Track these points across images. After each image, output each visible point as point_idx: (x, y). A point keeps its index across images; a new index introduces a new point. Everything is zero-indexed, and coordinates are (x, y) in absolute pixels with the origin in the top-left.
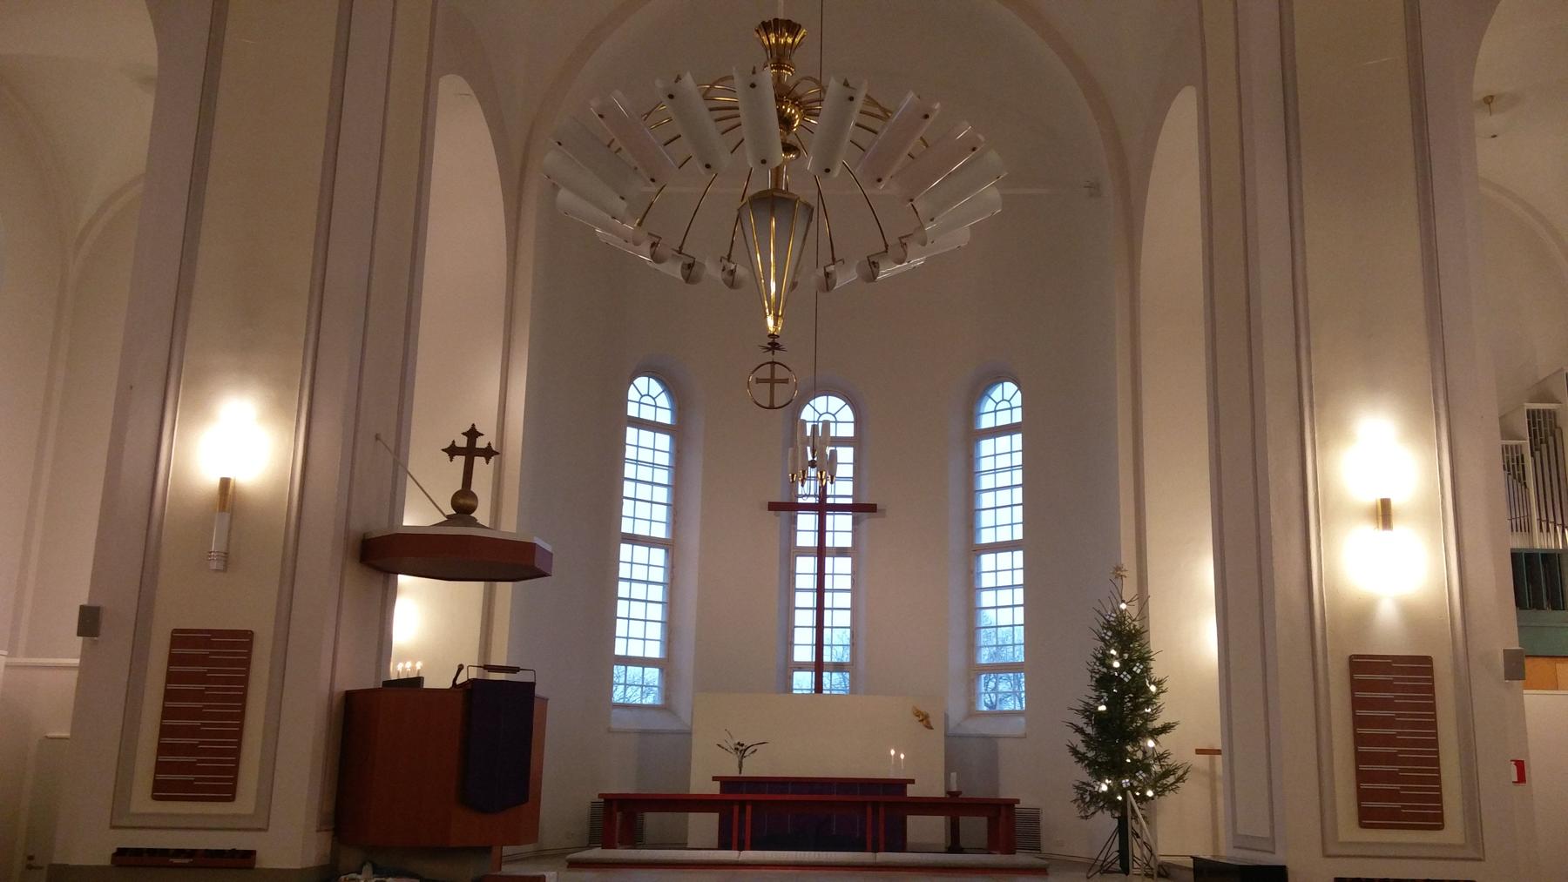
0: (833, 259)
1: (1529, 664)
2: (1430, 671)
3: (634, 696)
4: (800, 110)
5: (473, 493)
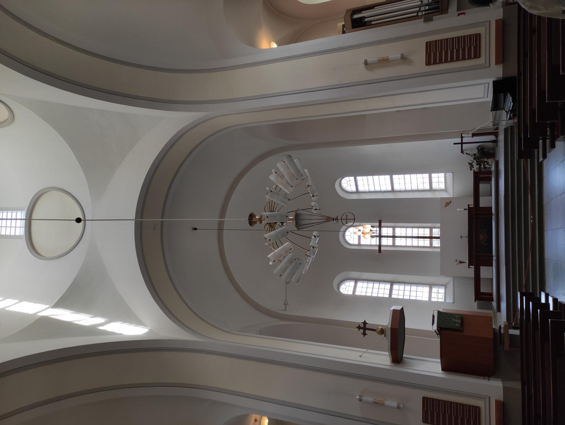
2: (430, 42)
3: (442, 179)
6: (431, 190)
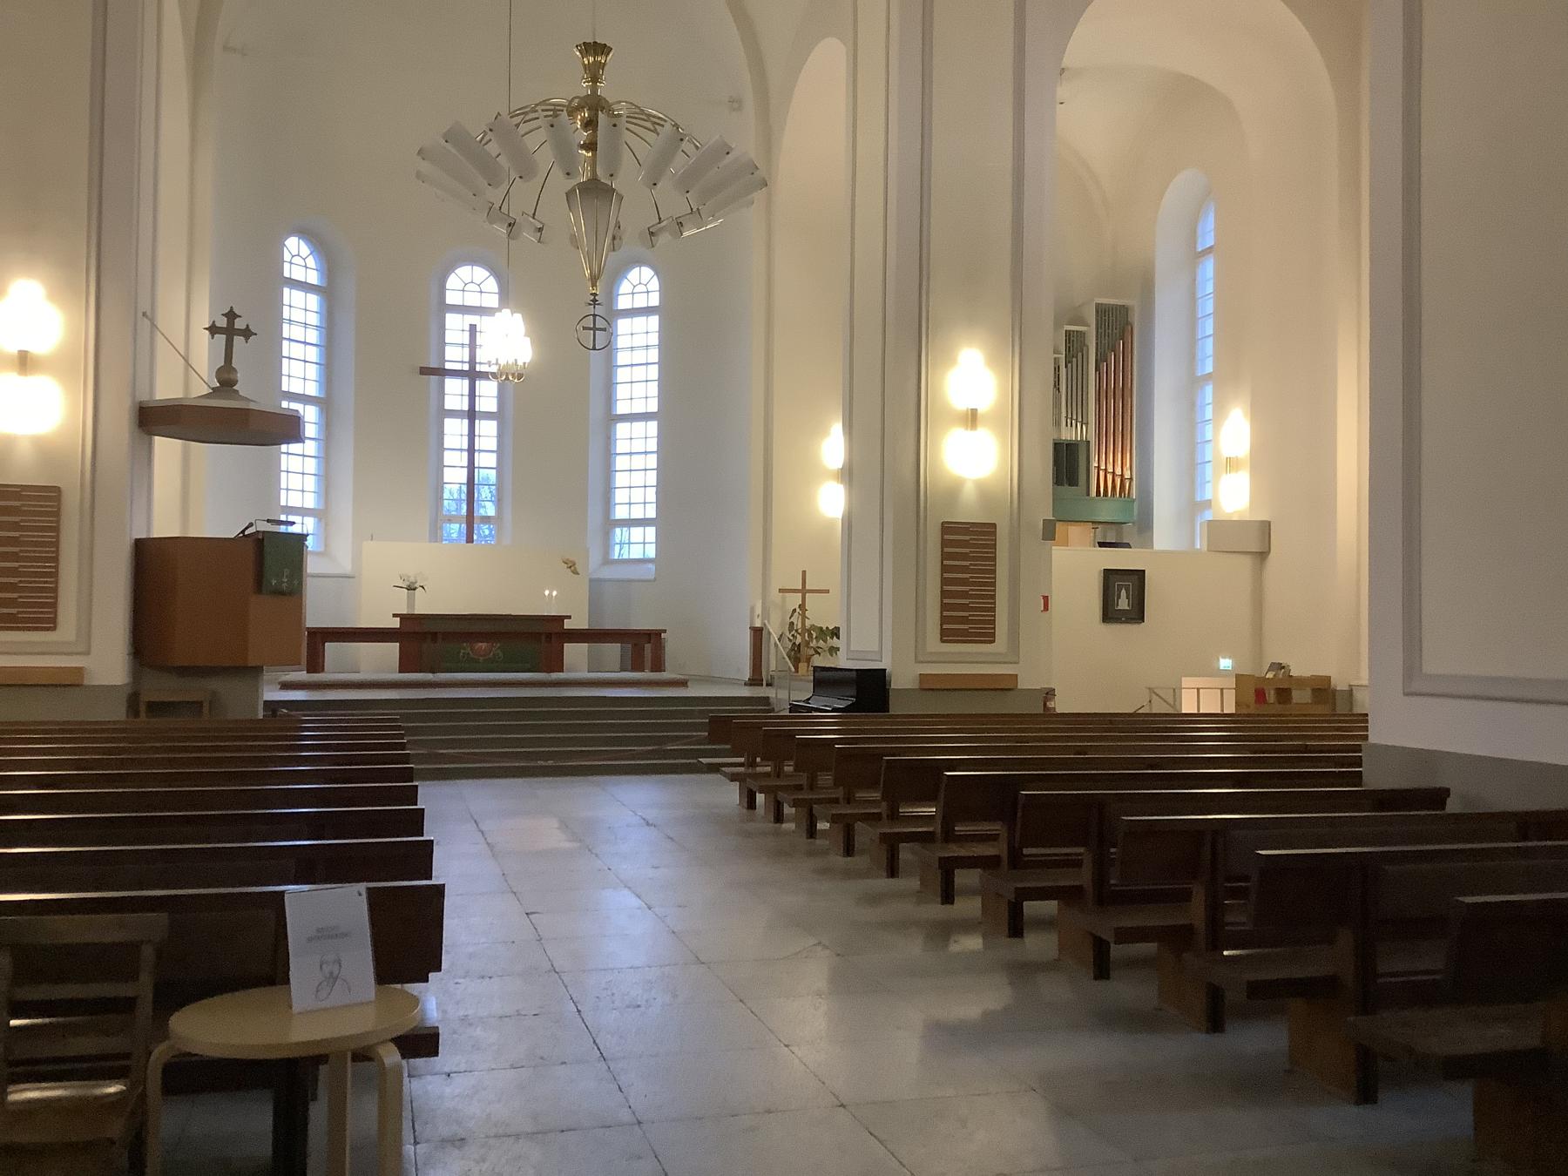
2: (994, 533)
3: (636, 553)
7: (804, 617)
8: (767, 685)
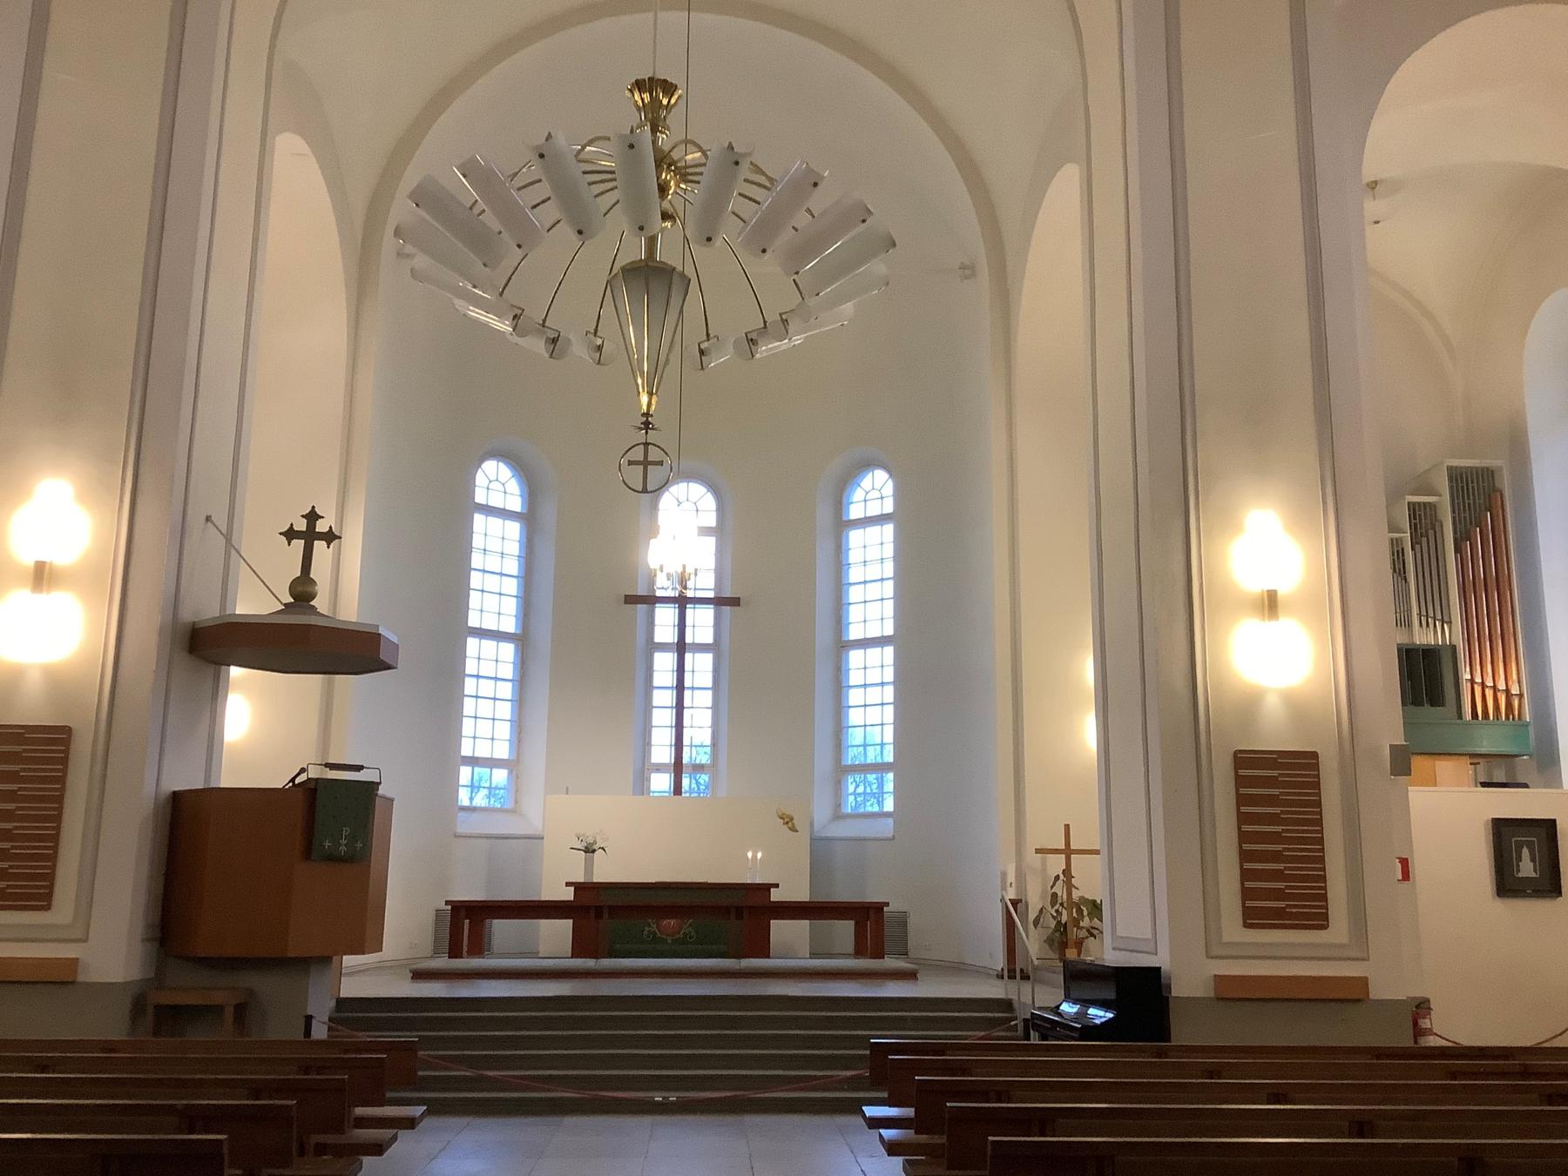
0: (708, 335)
1: (1418, 763)
2: (1316, 766)
4: (675, 176)
5: (312, 579)
6: (842, 771)
7: (1069, 886)
8: (1022, 978)
